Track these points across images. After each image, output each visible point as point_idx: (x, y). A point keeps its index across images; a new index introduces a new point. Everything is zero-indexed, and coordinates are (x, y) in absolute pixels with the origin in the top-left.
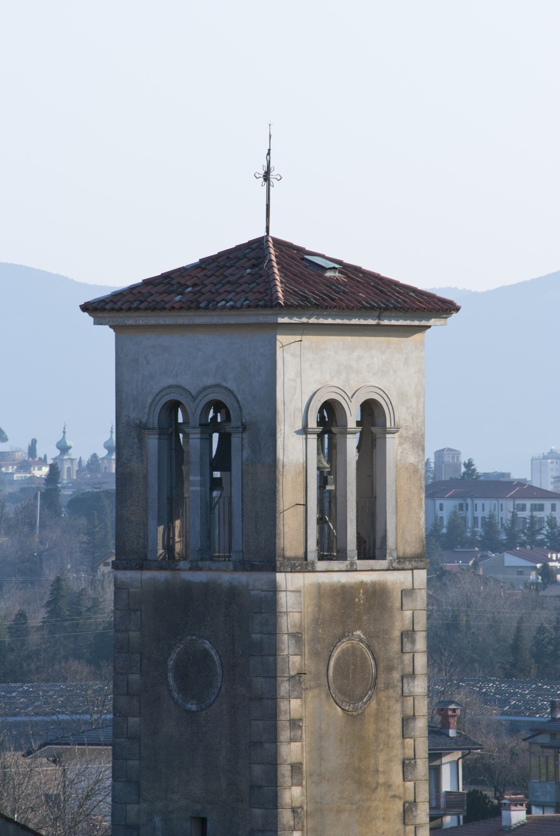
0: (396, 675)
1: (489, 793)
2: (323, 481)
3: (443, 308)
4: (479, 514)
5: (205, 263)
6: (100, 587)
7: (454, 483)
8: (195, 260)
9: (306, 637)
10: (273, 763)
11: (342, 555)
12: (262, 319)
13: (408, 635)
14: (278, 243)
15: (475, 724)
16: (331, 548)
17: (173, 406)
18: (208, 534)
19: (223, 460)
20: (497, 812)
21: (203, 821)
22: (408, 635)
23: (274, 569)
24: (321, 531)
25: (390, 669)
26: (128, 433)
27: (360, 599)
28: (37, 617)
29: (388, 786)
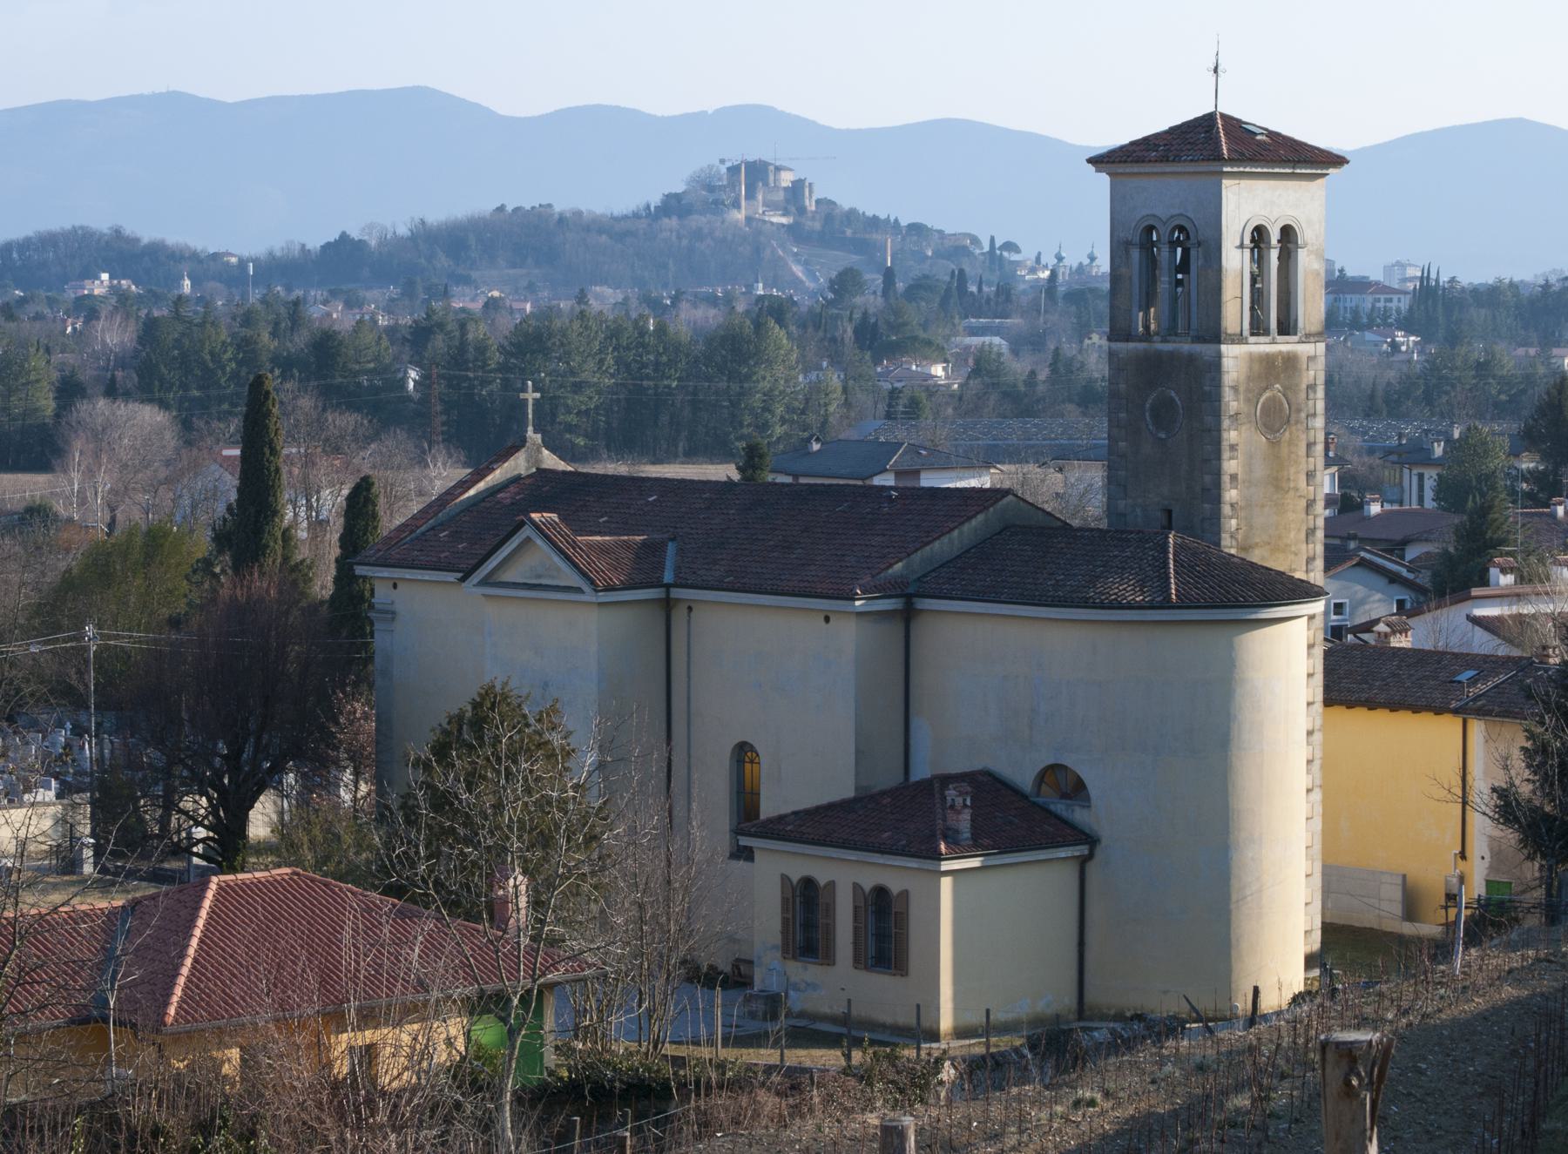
0: (1303, 415)
1: (1355, 494)
2: (1254, 280)
3: (1337, 161)
4: (1348, 305)
5: (1173, 130)
6: (1094, 354)
7: (1339, 285)
8: (1165, 127)
9: (1242, 389)
10: (1218, 473)
11: (1267, 332)
12: (1212, 169)
13: (1312, 387)
14: (1223, 116)
15: (1345, 448)
16: (1258, 328)
17: (1150, 229)
18: (1173, 318)
19: (1184, 267)
20: (1360, 506)
21: (1169, 512)
22: (1312, 387)
23: (1219, 342)
24: (1252, 316)
25: (1299, 411)
26: (1119, 248)
27: (1279, 362)
28: (1043, 374)
29: (1297, 489)
